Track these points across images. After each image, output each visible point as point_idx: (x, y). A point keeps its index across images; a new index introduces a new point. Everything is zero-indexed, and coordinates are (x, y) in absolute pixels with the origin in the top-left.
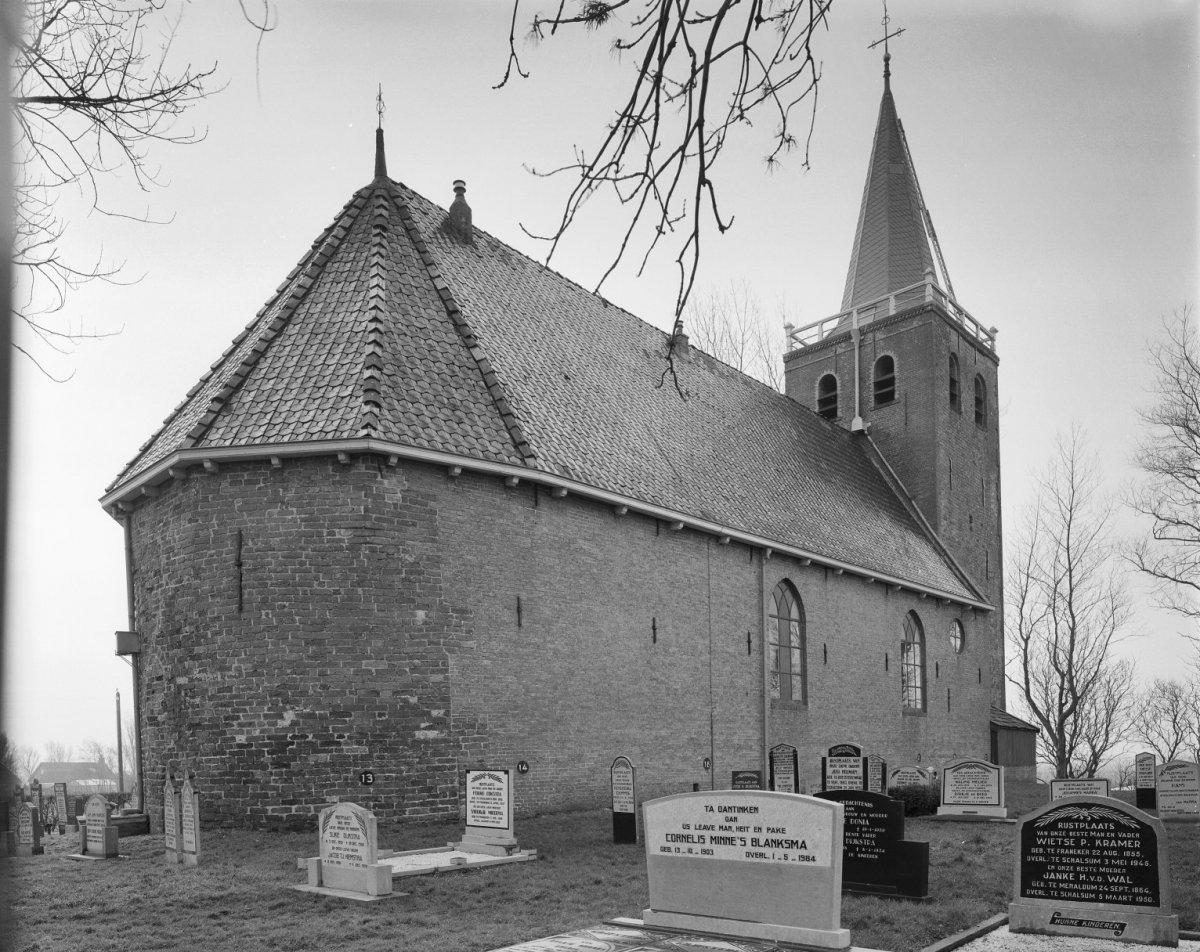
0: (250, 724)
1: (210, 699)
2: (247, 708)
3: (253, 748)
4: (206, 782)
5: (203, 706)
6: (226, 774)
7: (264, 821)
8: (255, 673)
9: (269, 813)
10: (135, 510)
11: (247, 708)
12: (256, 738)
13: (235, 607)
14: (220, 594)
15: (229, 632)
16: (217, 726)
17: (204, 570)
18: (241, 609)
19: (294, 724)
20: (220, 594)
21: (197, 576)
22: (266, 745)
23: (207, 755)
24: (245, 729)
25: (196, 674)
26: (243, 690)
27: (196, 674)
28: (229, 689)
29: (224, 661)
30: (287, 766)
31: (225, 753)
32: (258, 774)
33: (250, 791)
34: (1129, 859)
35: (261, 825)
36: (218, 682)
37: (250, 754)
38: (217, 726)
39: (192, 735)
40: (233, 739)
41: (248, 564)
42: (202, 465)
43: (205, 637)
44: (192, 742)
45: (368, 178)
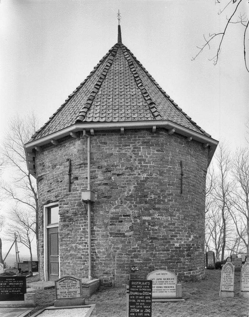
0: (181, 239)
1: (164, 227)
2: (181, 232)
3: (181, 249)
4: (158, 262)
5: (160, 230)
6: (168, 259)
7: (183, 278)
8: (184, 219)
9: (185, 275)
10: (57, 146)
11: (181, 232)
12: (182, 245)
13: (179, 191)
14: (173, 184)
15: (175, 201)
16: (166, 239)
17: (165, 173)
18: (181, 193)
19: (193, 240)
20: (173, 184)
21: (161, 175)
22: (185, 248)
23: (159, 251)
24: (179, 241)
25: (156, 216)
26: (179, 225)
27: (156, 216)
28: (174, 224)
29: (173, 212)
30: (190, 256)
31: (169, 251)
32: (182, 259)
33: (179, 266)
34: (139, 288)
35: (182, 280)
36: (169, 221)
37: (180, 251)
38: (166, 239)
39: (152, 242)
40: (174, 245)
41: (185, 175)
42: (90, 131)
43: (164, 201)
44: (150, 245)
45: (117, 42)
